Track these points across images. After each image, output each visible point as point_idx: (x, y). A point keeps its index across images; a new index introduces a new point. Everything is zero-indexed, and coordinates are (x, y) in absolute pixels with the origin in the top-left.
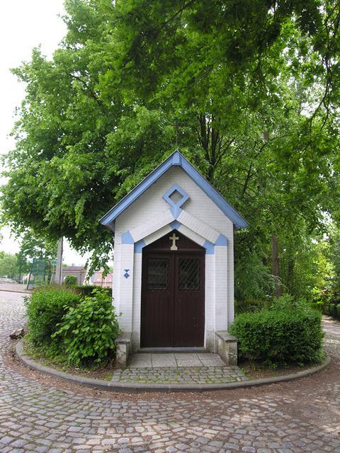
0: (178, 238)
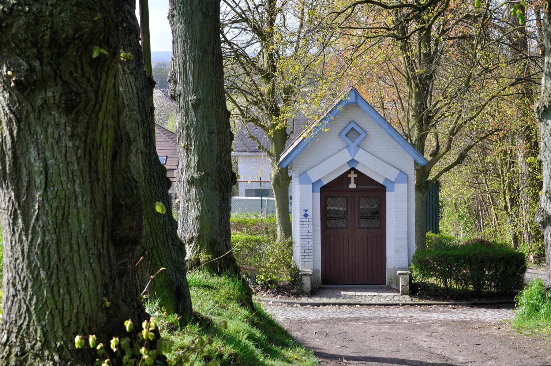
0: (356, 176)
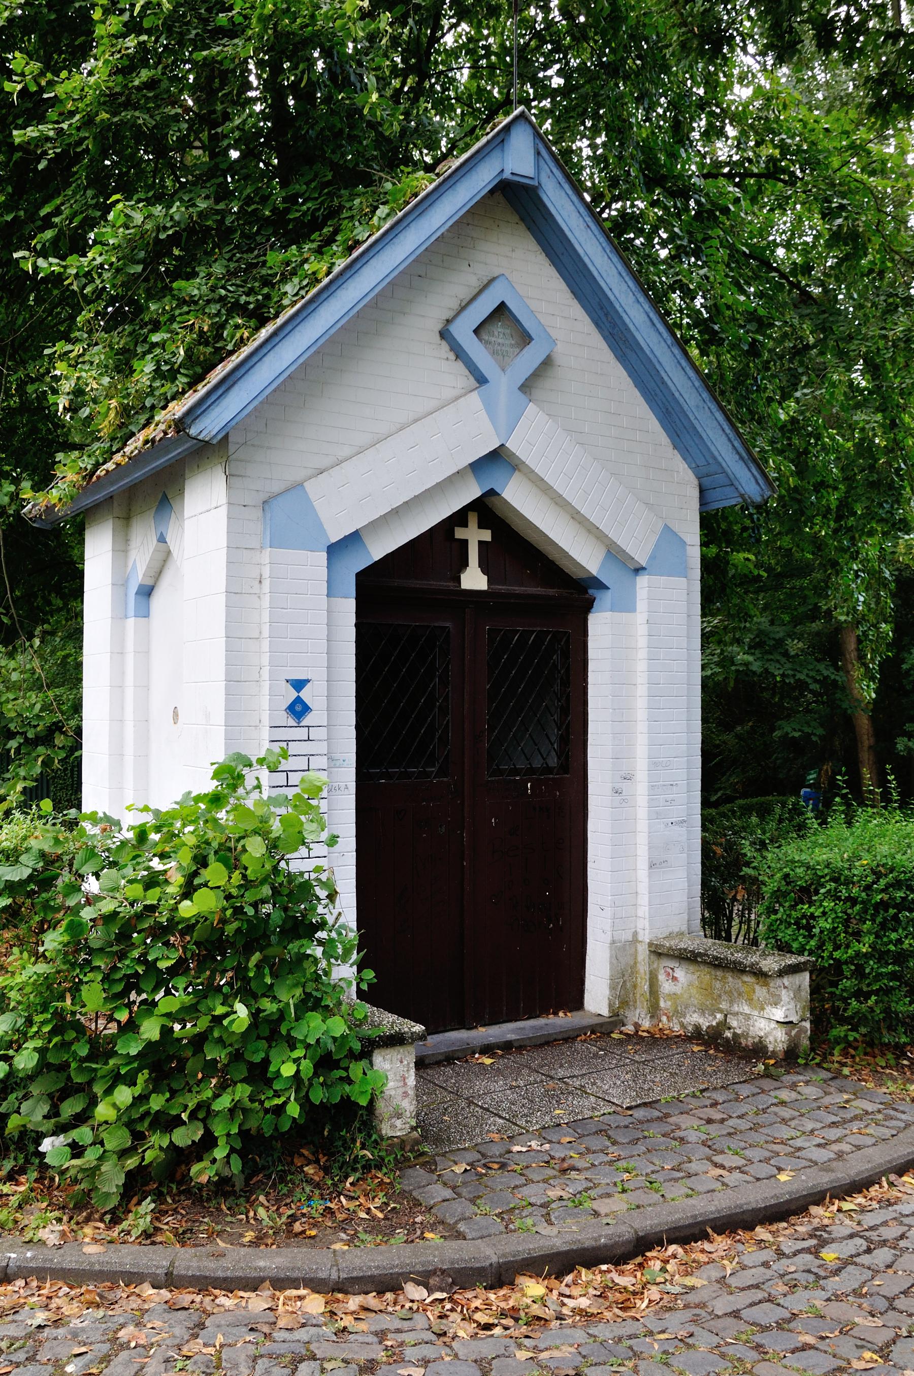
0: (487, 536)
